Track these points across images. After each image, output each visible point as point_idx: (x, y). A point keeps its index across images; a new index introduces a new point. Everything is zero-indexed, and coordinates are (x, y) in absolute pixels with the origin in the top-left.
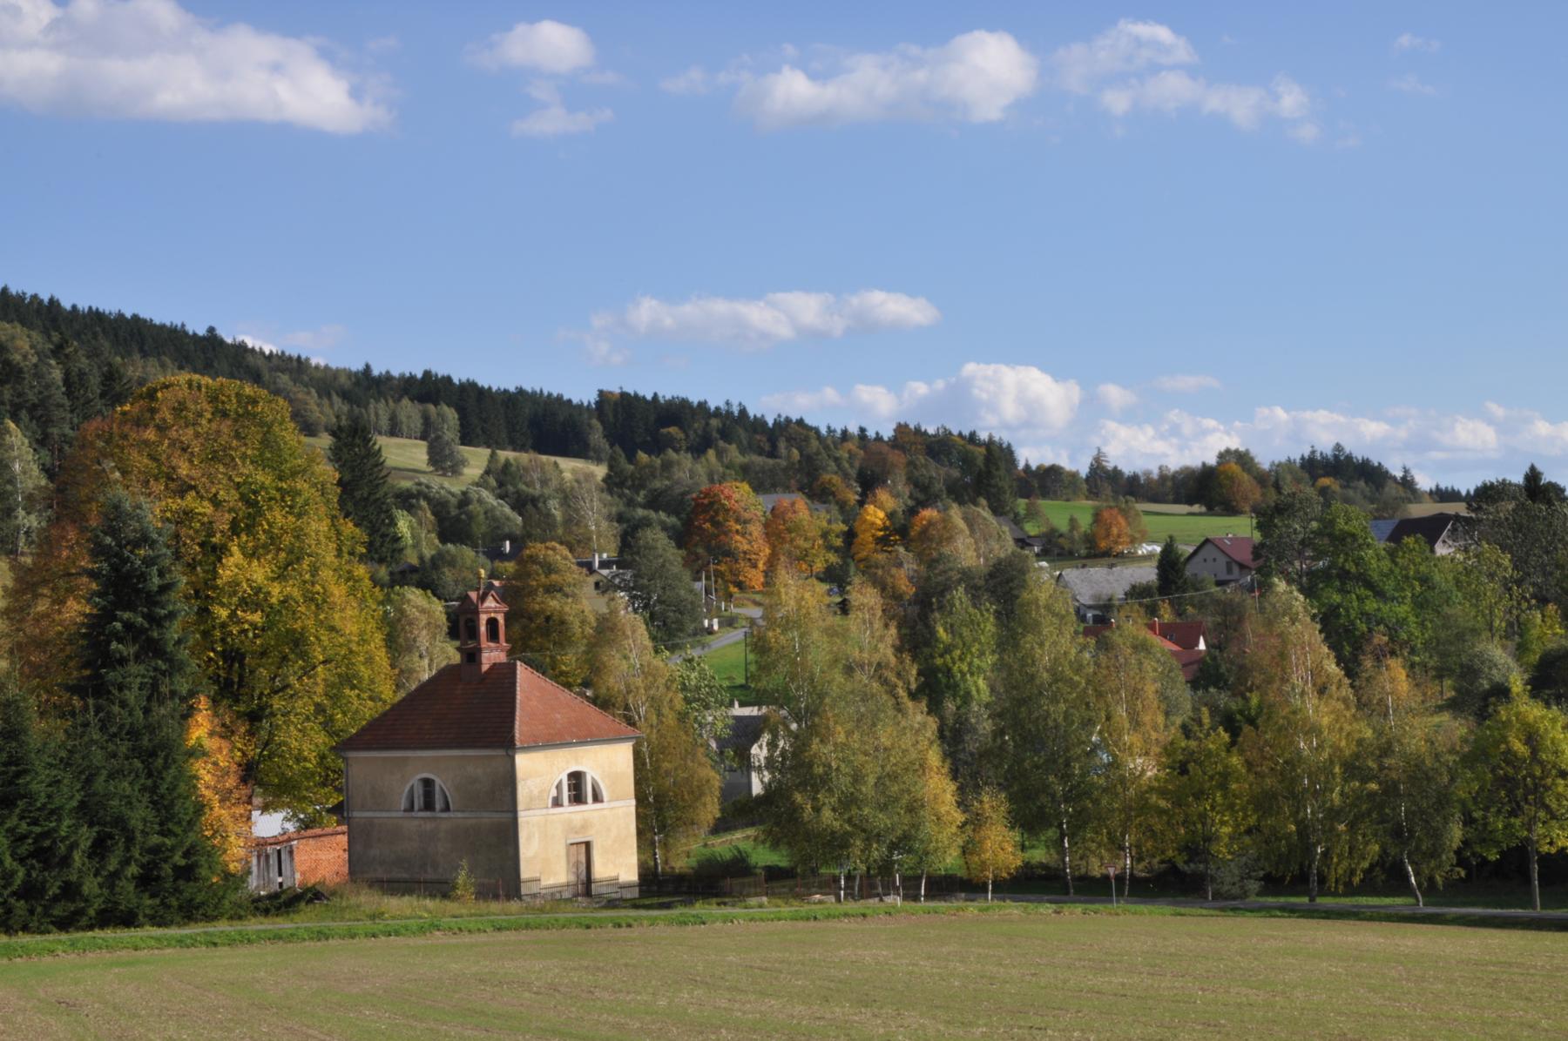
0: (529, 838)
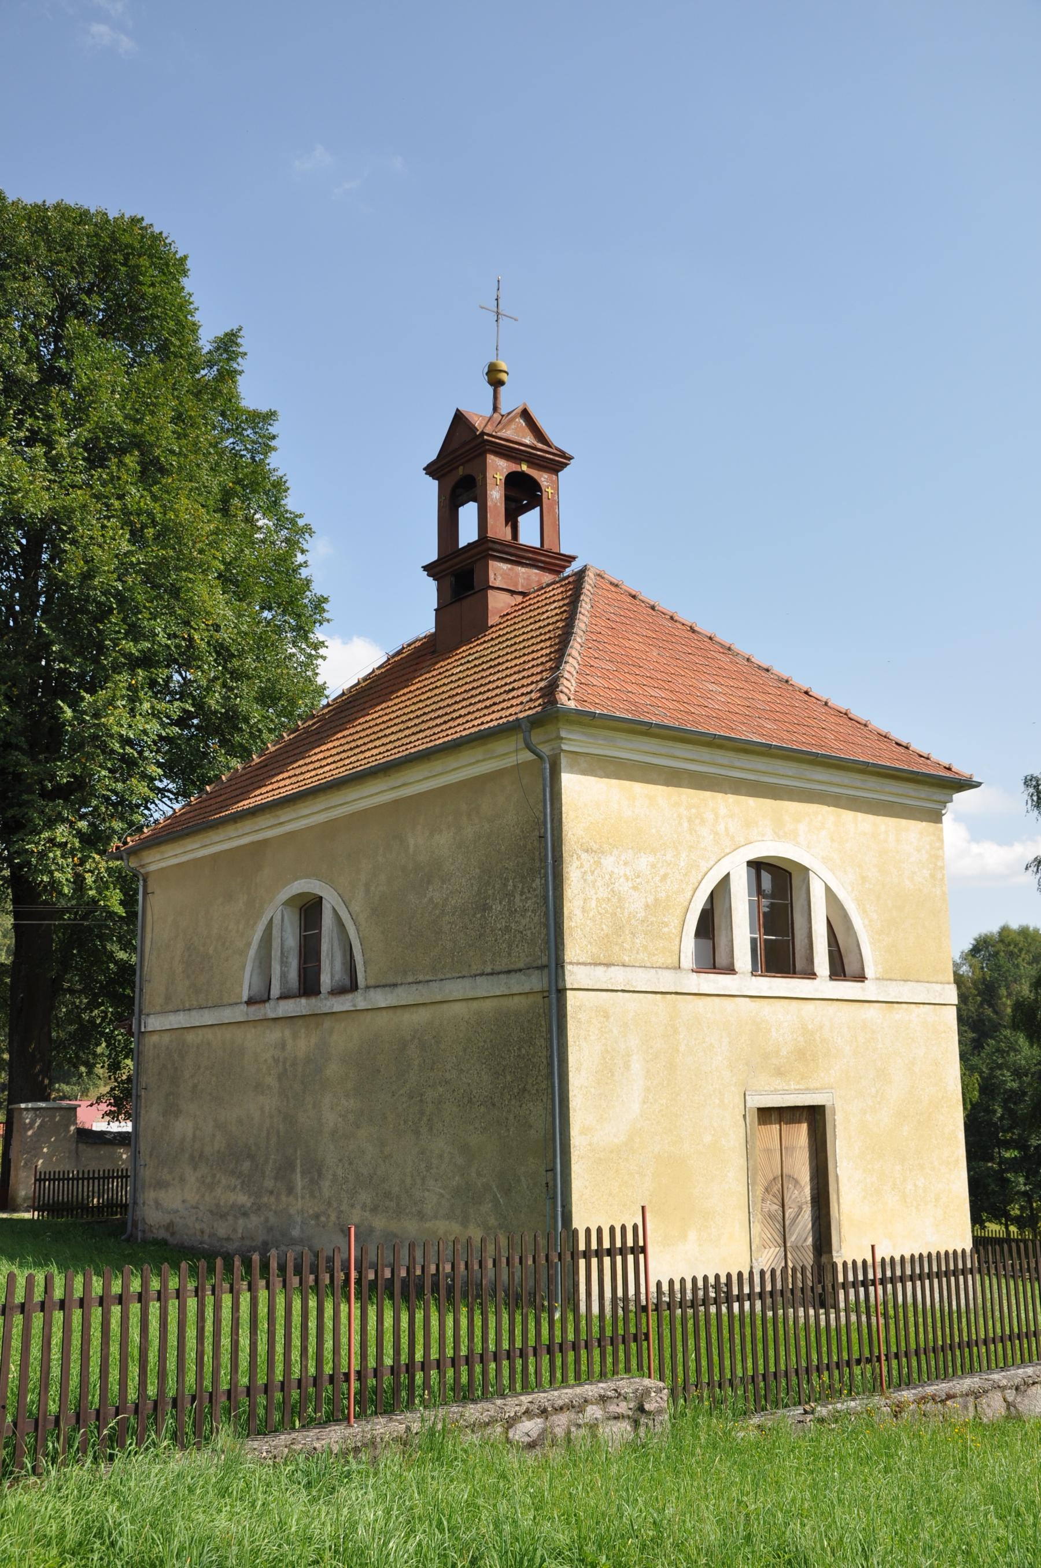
0: (578, 1070)
